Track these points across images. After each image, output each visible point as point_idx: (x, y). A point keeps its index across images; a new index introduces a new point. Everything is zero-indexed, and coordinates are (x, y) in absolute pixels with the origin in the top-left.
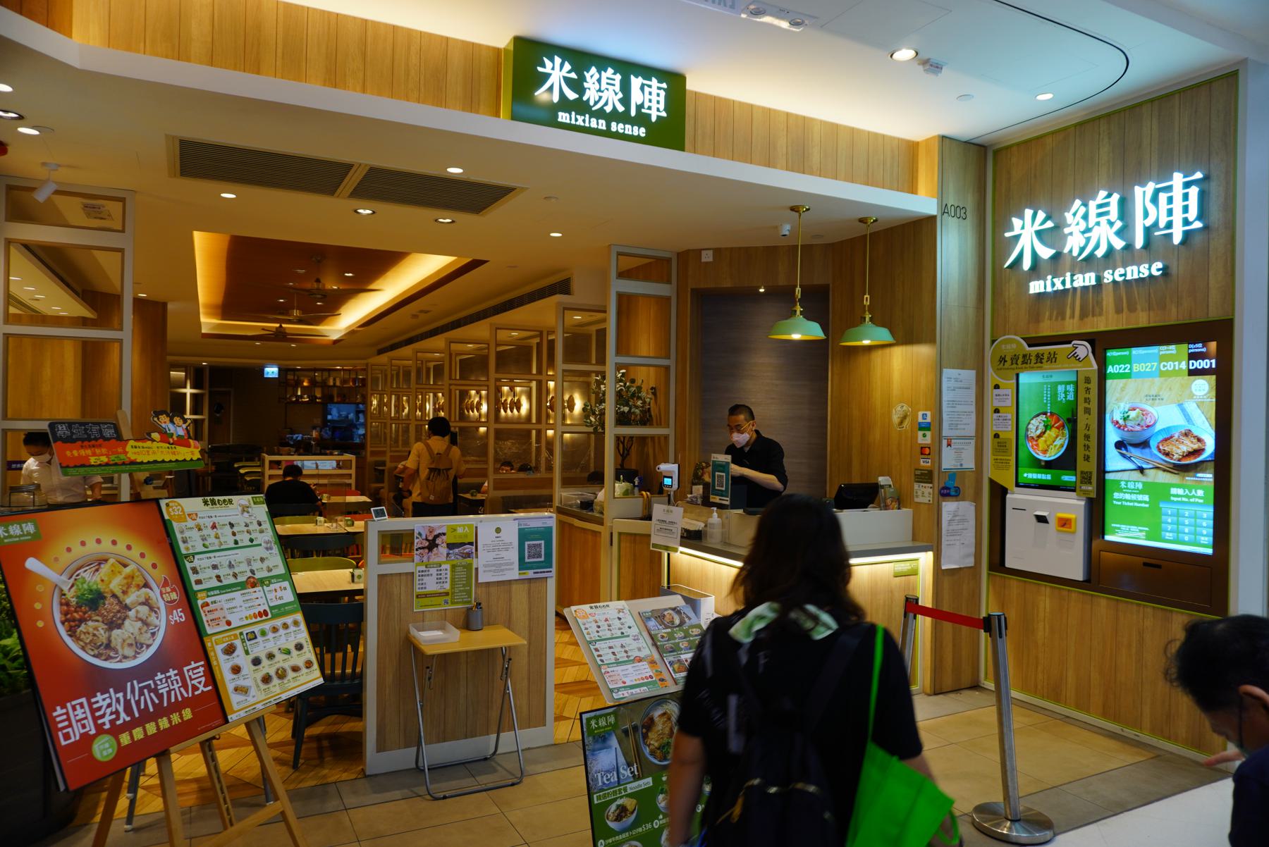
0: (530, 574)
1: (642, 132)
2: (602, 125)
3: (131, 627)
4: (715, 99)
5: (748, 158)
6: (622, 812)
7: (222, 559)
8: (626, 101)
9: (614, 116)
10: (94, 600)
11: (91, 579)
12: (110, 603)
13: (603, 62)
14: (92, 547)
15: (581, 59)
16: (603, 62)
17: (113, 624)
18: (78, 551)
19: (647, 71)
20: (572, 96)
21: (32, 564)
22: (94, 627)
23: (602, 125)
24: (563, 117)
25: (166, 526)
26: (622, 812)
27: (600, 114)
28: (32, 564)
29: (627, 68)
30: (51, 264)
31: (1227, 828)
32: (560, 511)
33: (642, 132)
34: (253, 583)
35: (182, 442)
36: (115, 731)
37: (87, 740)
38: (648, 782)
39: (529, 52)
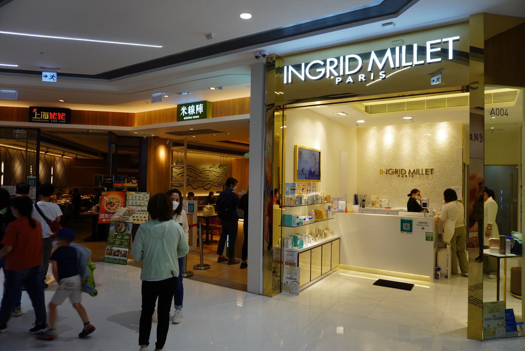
0: (190, 213)
1: (198, 117)
2: (191, 118)
3: (114, 207)
4: (221, 102)
5: (228, 114)
6: (112, 236)
7: (135, 201)
8: (195, 111)
9: (194, 115)
10: (111, 203)
11: (111, 200)
12: (113, 204)
13: (190, 104)
14: (113, 197)
15: (187, 105)
16: (190, 104)
17: (112, 206)
18: (111, 197)
19: (198, 103)
20: (186, 113)
21: (105, 197)
22: (109, 206)
23: (191, 118)
24: (185, 118)
25: (126, 195)
26: (112, 236)
27: (191, 115)
28: (105, 197)
29: (195, 104)
31: (141, 304)
33: (198, 117)
34: (139, 206)
35: (135, 184)
36: (106, 219)
37: (102, 219)
38: (117, 233)
39: (180, 106)
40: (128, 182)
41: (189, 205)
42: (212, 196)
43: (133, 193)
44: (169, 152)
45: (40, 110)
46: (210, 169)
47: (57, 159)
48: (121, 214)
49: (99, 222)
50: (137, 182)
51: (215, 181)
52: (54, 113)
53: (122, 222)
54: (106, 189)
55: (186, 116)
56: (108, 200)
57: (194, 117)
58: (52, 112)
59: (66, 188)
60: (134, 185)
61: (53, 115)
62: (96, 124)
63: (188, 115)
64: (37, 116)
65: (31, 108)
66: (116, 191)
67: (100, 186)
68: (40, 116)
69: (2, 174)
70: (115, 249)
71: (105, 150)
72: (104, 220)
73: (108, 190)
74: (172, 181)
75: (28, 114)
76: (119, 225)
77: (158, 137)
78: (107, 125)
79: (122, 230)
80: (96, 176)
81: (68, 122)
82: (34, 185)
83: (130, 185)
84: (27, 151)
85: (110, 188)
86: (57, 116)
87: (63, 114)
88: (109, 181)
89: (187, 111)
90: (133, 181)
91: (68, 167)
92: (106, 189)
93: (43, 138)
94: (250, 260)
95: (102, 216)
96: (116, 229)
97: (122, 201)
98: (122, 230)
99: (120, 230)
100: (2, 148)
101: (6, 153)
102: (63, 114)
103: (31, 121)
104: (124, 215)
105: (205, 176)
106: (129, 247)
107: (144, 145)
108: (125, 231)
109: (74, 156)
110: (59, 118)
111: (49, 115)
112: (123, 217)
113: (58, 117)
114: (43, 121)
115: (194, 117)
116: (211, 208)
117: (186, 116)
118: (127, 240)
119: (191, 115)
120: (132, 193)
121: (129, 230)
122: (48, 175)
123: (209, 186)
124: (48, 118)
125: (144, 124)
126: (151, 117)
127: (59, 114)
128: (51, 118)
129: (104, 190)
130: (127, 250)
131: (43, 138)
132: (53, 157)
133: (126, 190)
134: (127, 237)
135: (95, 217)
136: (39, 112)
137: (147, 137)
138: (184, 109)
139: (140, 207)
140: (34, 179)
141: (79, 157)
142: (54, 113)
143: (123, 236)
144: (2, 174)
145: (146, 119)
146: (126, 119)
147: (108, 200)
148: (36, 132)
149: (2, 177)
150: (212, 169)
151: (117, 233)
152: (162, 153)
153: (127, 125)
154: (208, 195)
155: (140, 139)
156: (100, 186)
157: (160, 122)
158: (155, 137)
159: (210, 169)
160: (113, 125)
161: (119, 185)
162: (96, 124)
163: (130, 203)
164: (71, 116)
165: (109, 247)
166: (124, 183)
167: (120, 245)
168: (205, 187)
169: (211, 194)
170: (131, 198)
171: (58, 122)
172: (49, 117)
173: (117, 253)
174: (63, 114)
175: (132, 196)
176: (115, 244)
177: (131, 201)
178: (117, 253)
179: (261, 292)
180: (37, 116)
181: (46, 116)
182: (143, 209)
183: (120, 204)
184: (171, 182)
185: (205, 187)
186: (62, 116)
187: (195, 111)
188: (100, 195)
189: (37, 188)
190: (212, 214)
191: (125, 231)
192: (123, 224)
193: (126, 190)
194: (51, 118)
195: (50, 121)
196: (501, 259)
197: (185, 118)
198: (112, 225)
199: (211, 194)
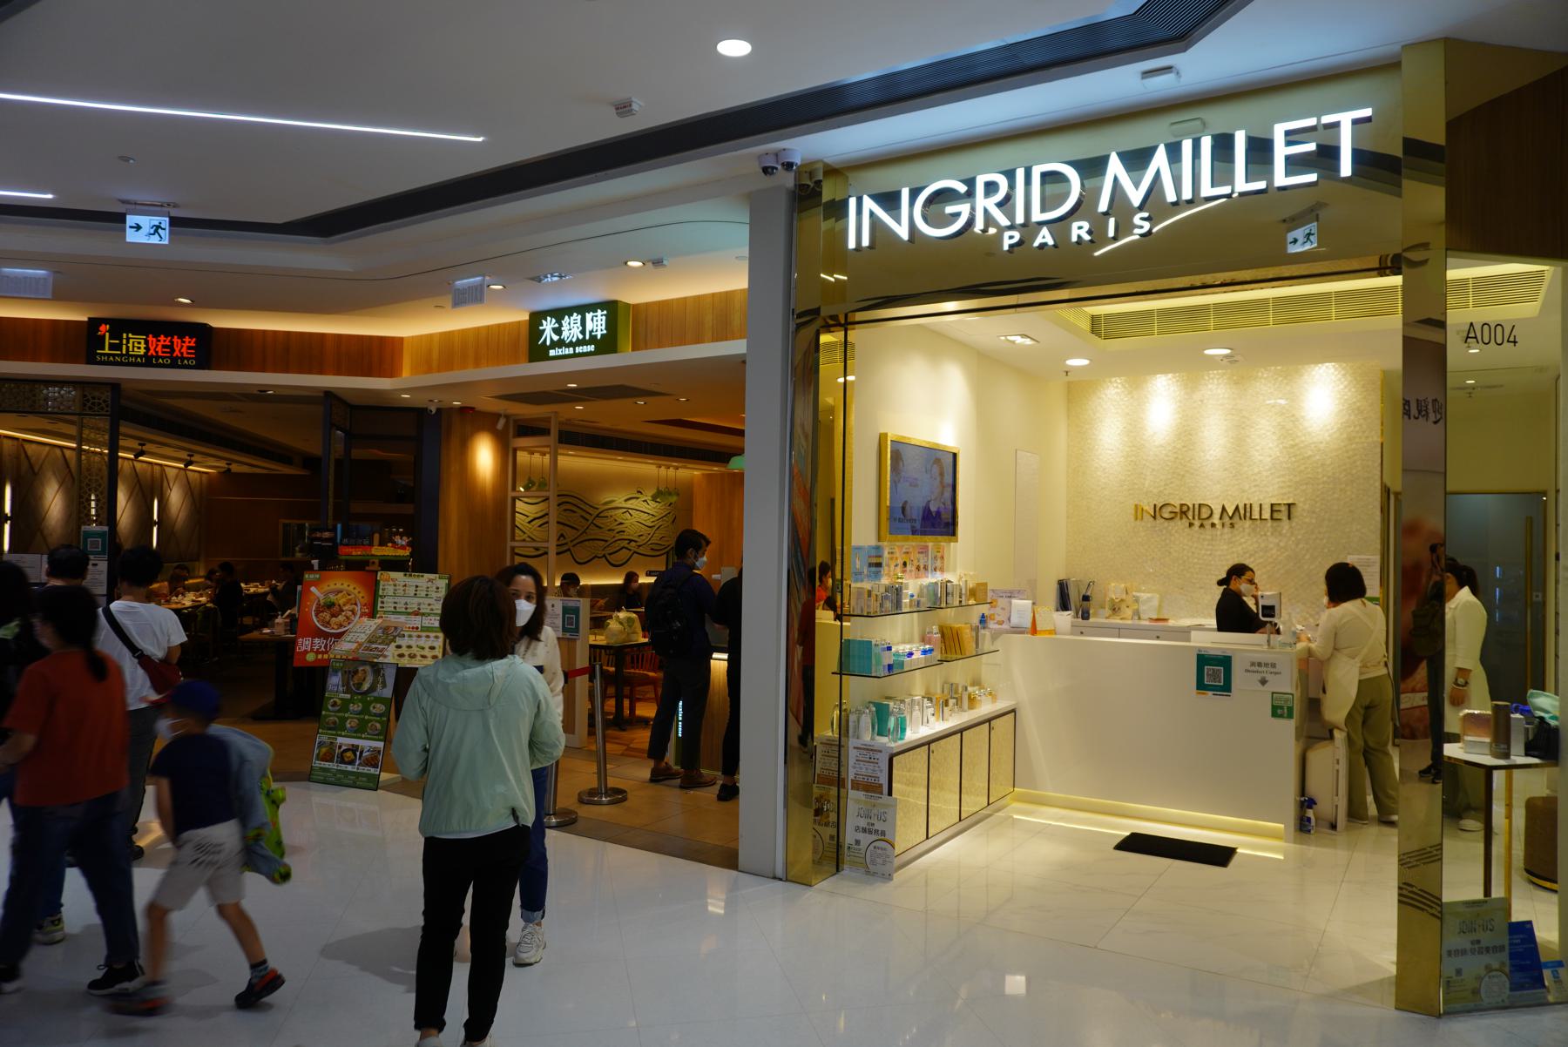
0: (568, 635)
1: (591, 348)
2: (571, 351)
3: (341, 618)
4: (659, 303)
5: (682, 341)
6: (335, 704)
7: (403, 600)
8: (583, 332)
9: (580, 343)
10: (330, 606)
11: (332, 598)
12: (336, 608)
13: (569, 311)
14: (339, 586)
15: (559, 314)
16: (569, 311)
17: (334, 615)
18: (332, 587)
19: (593, 307)
20: (556, 338)
21: (313, 589)
22: (326, 615)
23: (571, 351)
24: (552, 353)
25: (377, 583)
26: (335, 704)
27: (571, 344)
28: (313, 589)
29: (582, 309)
30: (1355, 265)
31: (422, 908)
32: (917, 607)
33: (591, 348)
34: (416, 613)
35: (403, 547)
36: (317, 652)
37: (306, 652)
38: (348, 696)
39: (537, 317)
40: (382, 544)
41: (566, 610)
42: (634, 585)
43: (398, 575)
44: (506, 453)
45: (120, 327)
46: (629, 504)
47: (171, 473)
48: (363, 638)
49: (297, 663)
50: (409, 544)
51: (641, 541)
52: (162, 338)
53: (364, 663)
54: (315, 562)
55: (554, 345)
56: (321, 597)
57: (578, 350)
58: (156, 335)
59: (198, 559)
60: (401, 553)
61: (159, 344)
62: (287, 371)
63: (561, 343)
64: (112, 347)
65: (94, 323)
66: (347, 569)
67: (298, 555)
68: (119, 347)
69: (6, 518)
70: (344, 741)
71: (314, 447)
72: (310, 657)
73: (322, 568)
74: (513, 539)
75: (83, 341)
76: (356, 672)
77: (472, 409)
78: (321, 372)
79: (366, 686)
80: (285, 525)
81: (203, 363)
82: (103, 552)
83: (388, 551)
84: (79, 451)
85: (330, 560)
86: (171, 347)
87: (187, 339)
88: (326, 540)
89: (558, 331)
90: (397, 539)
91: (203, 499)
92: (315, 562)
93: (127, 412)
94: (746, 776)
95: (304, 644)
96: (346, 684)
97: (364, 601)
98: (366, 686)
99: (359, 685)
100: (6, 441)
101: (18, 458)
102: (190, 342)
103: (91, 359)
104: (371, 642)
105: (613, 526)
106: (385, 735)
107: (429, 431)
108: (372, 689)
109: (222, 464)
110: (177, 353)
111: (146, 342)
112: (367, 649)
113: (173, 350)
114: (129, 361)
115: (578, 350)
116: (629, 620)
117: (554, 345)
118: (380, 715)
119: (571, 344)
120: (393, 575)
121: (384, 686)
122: (143, 521)
123: (624, 554)
124: (142, 351)
125: (429, 370)
126: (451, 350)
127: (175, 339)
128: (152, 352)
129: (310, 568)
130: (380, 745)
131: (127, 412)
132: (157, 468)
133: (376, 567)
134: (380, 708)
135: (285, 648)
136: (115, 334)
137: (439, 410)
138: (548, 325)
139: (419, 618)
140: (101, 535)
141: (235, 468)
142: (162, 338)
143: (366, 705)
144: (6, 518)
145: (435, 355)
146: (375, 355)
147: (321, 597)
148: (107, 395)
149: (7, 527)
150: (632, 504)
151: (348, 696)
152: (484, 457)
153: (381, 373)
154: (620, 581)
155: (419, 413)
156: (298, 555)
157: (477, 364)
158: (463, 410)
159: (629, 504)
160: (338, 372)
161: (356, 553)
162: (286, 370)
163: (389, 606)
164: (212, 347)
165: (325, 738)
166: (371, 545)
167: (359, 731)
168: (612, 559)
169: (631, 577)
170: (390, 590)
171: (174, 364)
172: (147, 349)
173: (349, 754)
174: (187, 339)
175: (394, 583)
176: (344, 728)
177: (391, 600)
178: (349, 754)
179: (779, 872)
180: (112, 347)
181: (136, 345)
182: (426, 622)
183: (358, 609)
184: (510, 544)
185: (612, 559)
186: (184, 346)
187: (583, 332)
188: (300, 581)
189: (109, 561)
190: (634, 637)
191: (372, 689)
192: (368, 668)
193: (376, 567)
194: (152, 352)
195: (148, 361)
196: (1496, 773)
197: (552, 353)
198: (336, 672)
199: (631, 577)
